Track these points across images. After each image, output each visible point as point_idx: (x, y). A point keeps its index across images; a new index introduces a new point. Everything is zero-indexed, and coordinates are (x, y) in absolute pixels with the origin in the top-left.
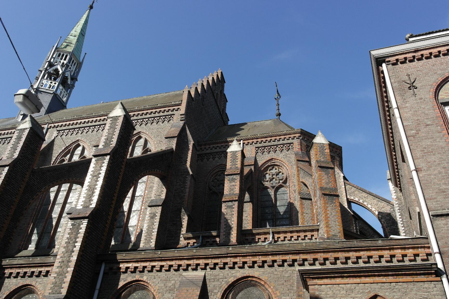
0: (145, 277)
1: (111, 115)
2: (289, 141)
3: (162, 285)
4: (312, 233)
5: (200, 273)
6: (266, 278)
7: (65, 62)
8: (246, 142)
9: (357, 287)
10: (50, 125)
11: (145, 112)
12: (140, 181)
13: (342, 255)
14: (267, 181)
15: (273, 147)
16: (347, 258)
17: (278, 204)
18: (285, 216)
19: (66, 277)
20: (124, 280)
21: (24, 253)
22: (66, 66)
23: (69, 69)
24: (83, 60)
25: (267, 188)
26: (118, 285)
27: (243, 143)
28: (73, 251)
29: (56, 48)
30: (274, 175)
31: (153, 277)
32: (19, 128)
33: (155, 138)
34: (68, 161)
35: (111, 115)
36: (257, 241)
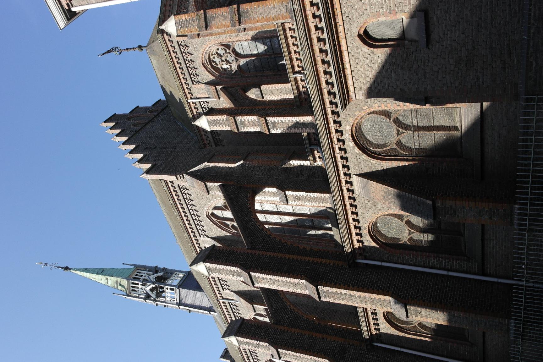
1: (206, 273)
2: (177, 46)
3: (370, 210)
4: (287, 29)
5: (355, 179)
7: (140, 283)
8: (189, 96)
9: (353, 54)
10: (219, 297)
11: (183, 214)
13: (317, 46)
14: (231, 66)
15: (188, 65)
16: (314, 16)
17: (255, 52)
18: (269, 43)
19: (375, 298)
20: (369, 242)
21: (337, 238)
22: (145, 282)
23: (147, 278)
24: (132, 265)
25: (239, 67)
26: (374, 247)
27: (191, 99)
29: (127, 295)
30: (221, 59)
31: (364, 219)
32: (237, 345)
33: (210, 199)
34: (234, 221)
35: (206, 273)
36: (305, 89)
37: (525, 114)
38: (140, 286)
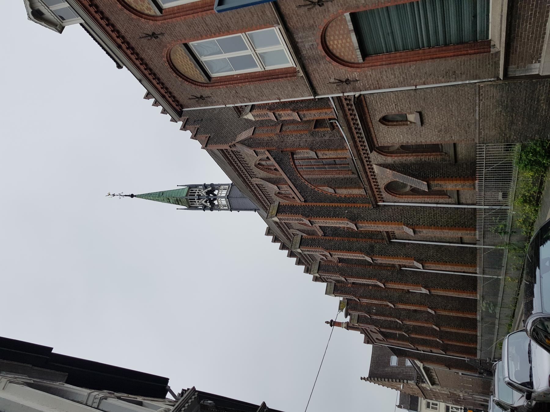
5: (374, 166)
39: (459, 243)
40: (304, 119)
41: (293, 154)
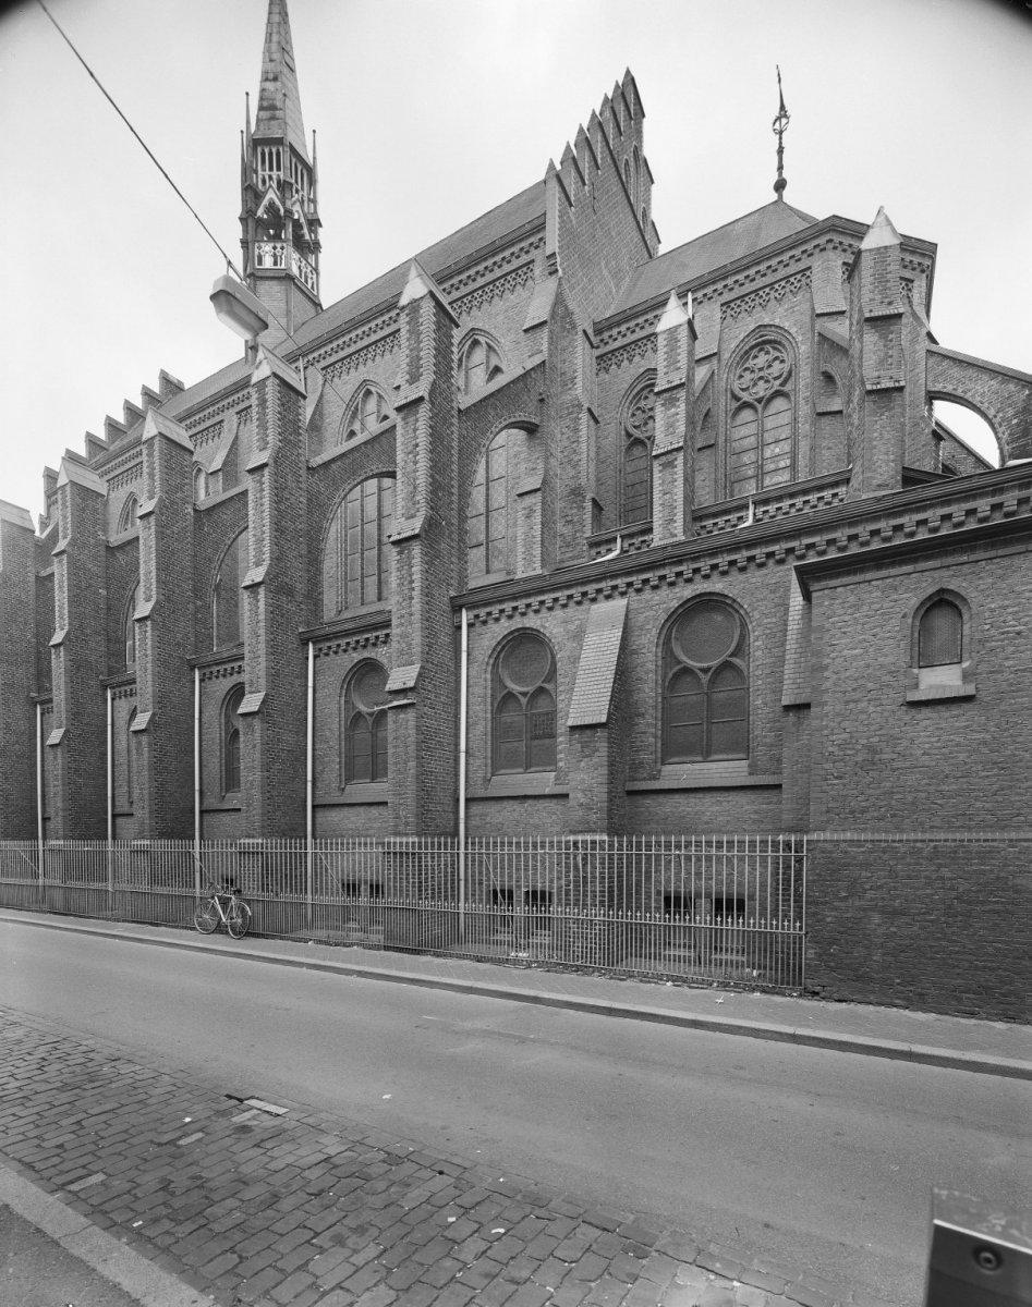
0: (532, 621)
1: (404, 301)
2: (801, 266)
5: (619, 604)
6: (736, 592)
8: (699, 295)
12: (494, 445)
24: (314, 158)
28: (411, 598)
35: (404, 301)
37: (551, 842)
38: (275, 174)
39: (113, 810)
40: (656, 464)
41: (531, 429)
